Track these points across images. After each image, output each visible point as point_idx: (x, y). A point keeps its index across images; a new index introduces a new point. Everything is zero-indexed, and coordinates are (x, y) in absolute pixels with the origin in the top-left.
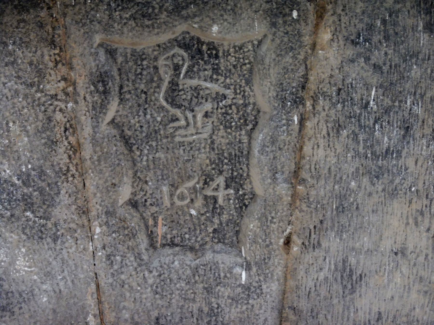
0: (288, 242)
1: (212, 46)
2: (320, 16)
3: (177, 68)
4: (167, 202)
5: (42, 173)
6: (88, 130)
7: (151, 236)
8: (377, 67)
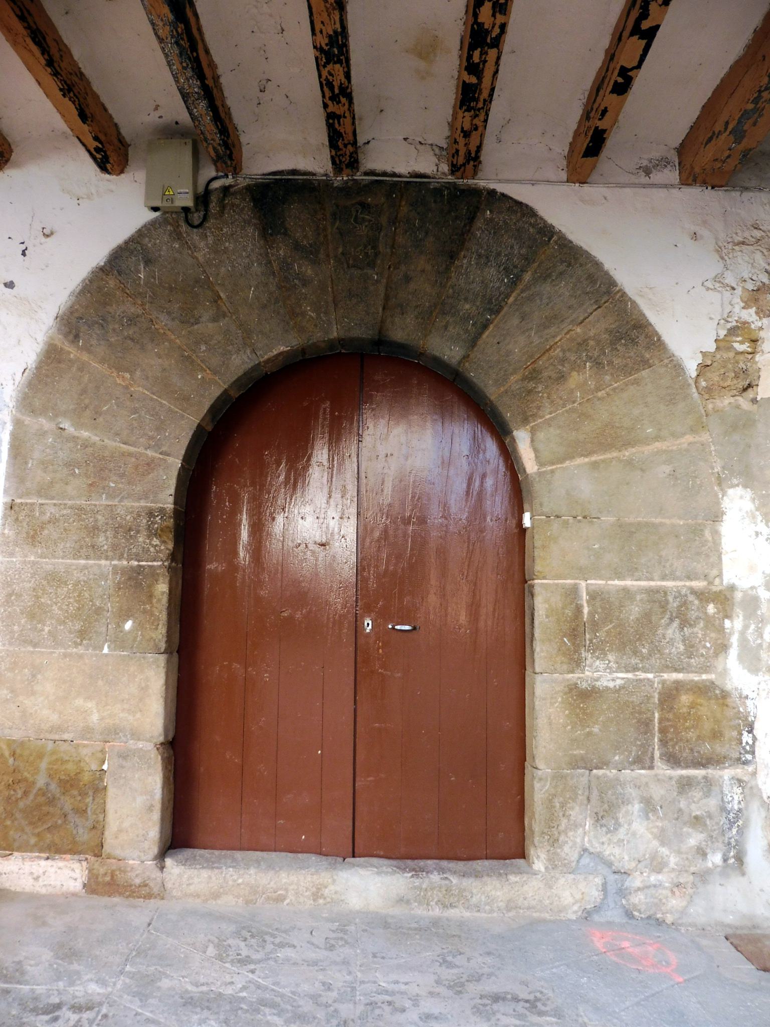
0: (390, 267)
1: (368, 205)
2: (402, 197)
3: (357, 211)
4: (353, 253)
5: (315, 243)
6: (330, 230)
7: (348, 264)
8: (418, 213)
